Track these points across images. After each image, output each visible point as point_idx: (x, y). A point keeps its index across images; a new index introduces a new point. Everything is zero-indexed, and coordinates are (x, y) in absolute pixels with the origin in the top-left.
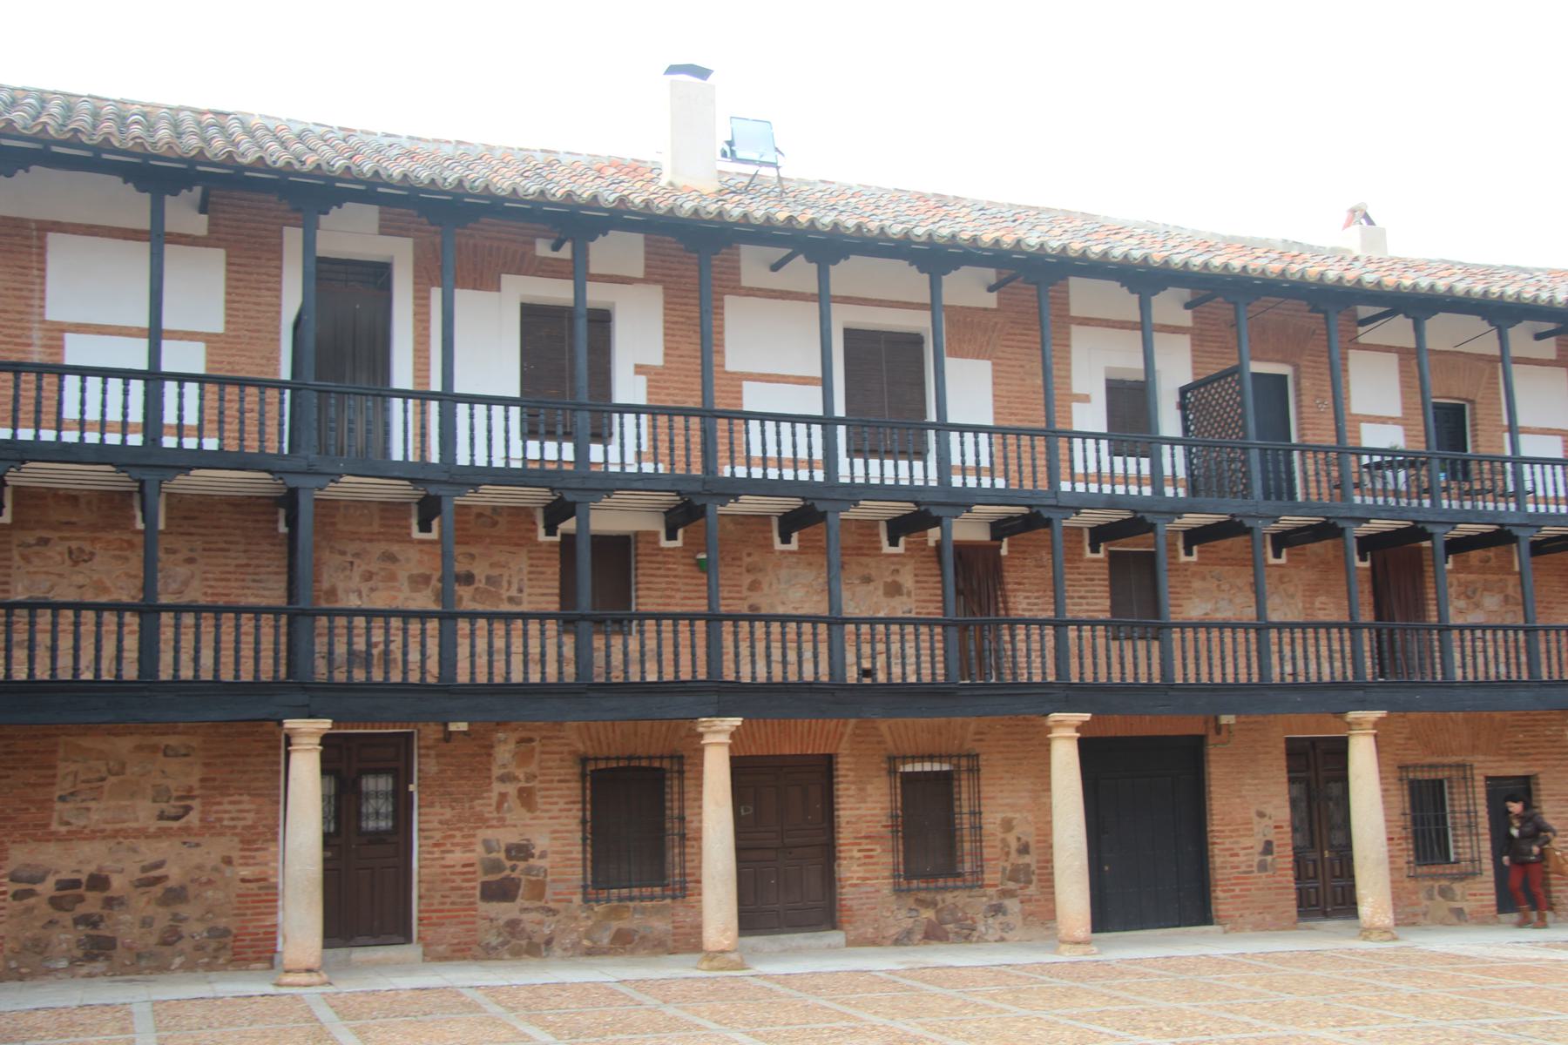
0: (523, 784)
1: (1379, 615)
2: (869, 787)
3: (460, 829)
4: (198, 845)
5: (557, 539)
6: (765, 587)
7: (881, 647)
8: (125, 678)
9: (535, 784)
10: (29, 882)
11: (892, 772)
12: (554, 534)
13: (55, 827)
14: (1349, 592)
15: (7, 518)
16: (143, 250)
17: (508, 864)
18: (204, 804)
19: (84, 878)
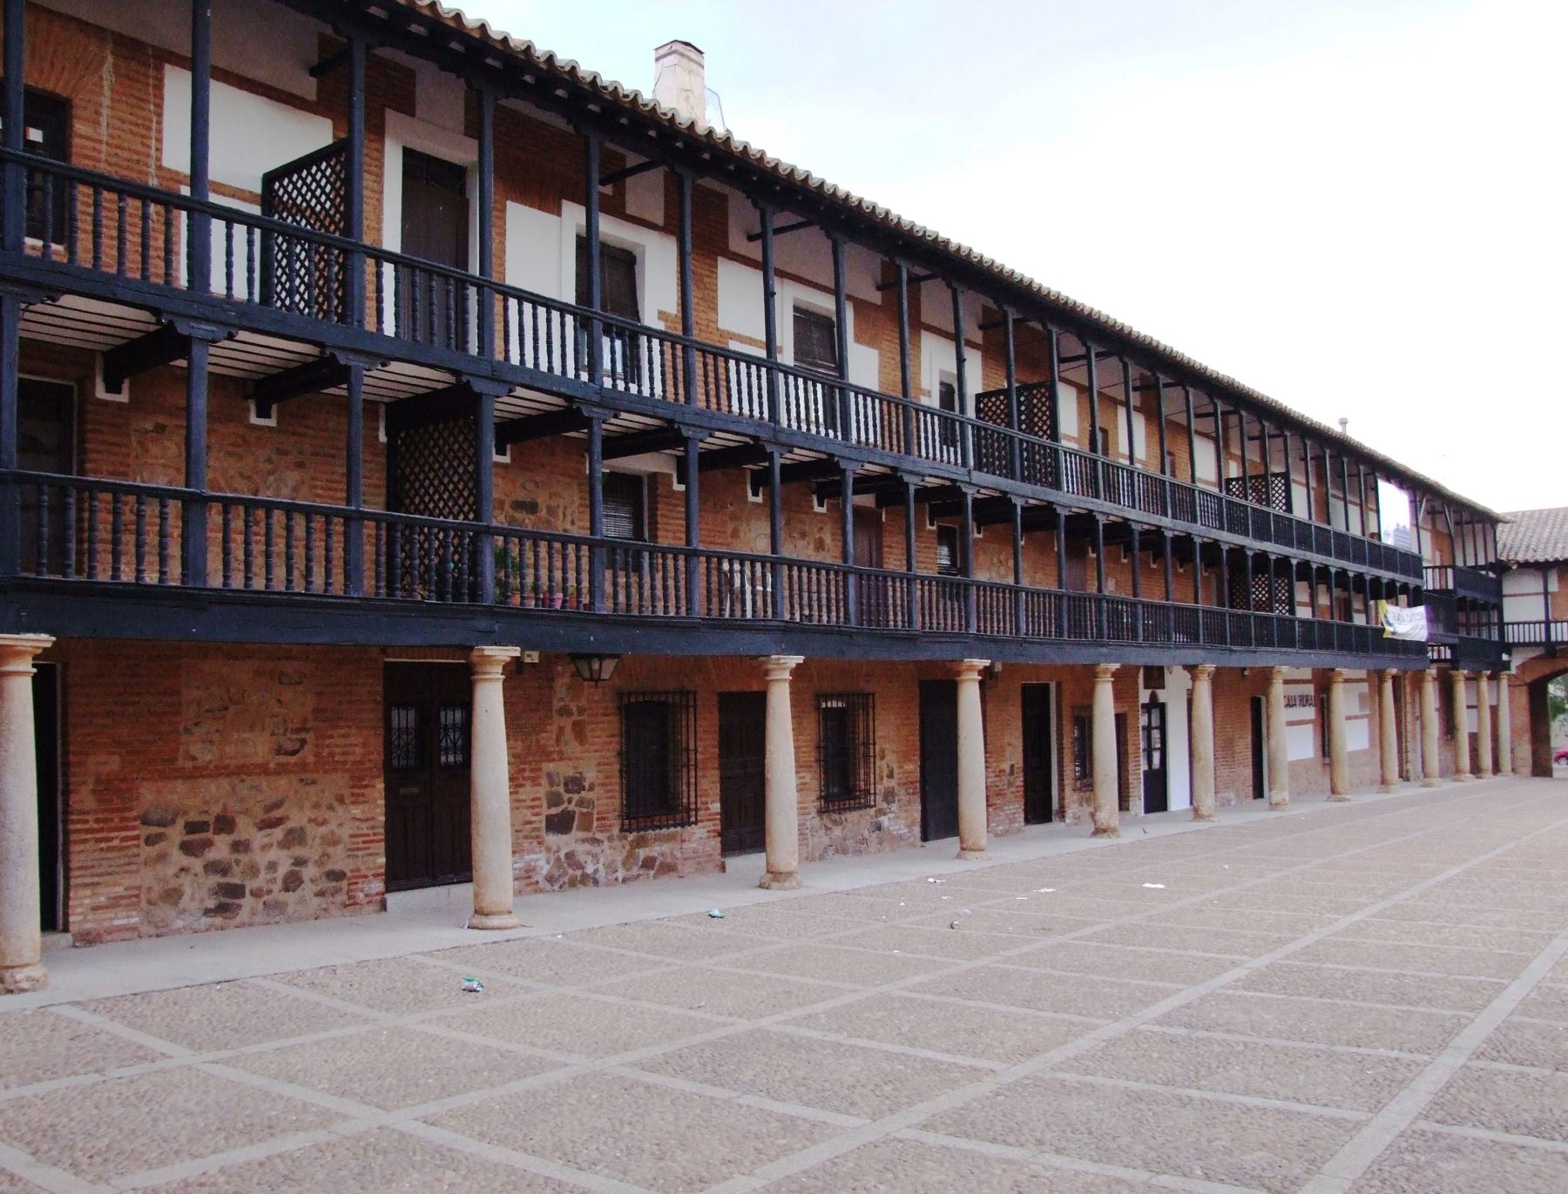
0: (576, 717)
1: (393, 502)
4: (314, 782)
9: (585, 717)
10: (159, 825)
11: (818, 708)
13: (180, 763)
14: (349, 475)
16: (758, 276)
17: (566, 796)
18: (317, 738)
19: (211, 819)
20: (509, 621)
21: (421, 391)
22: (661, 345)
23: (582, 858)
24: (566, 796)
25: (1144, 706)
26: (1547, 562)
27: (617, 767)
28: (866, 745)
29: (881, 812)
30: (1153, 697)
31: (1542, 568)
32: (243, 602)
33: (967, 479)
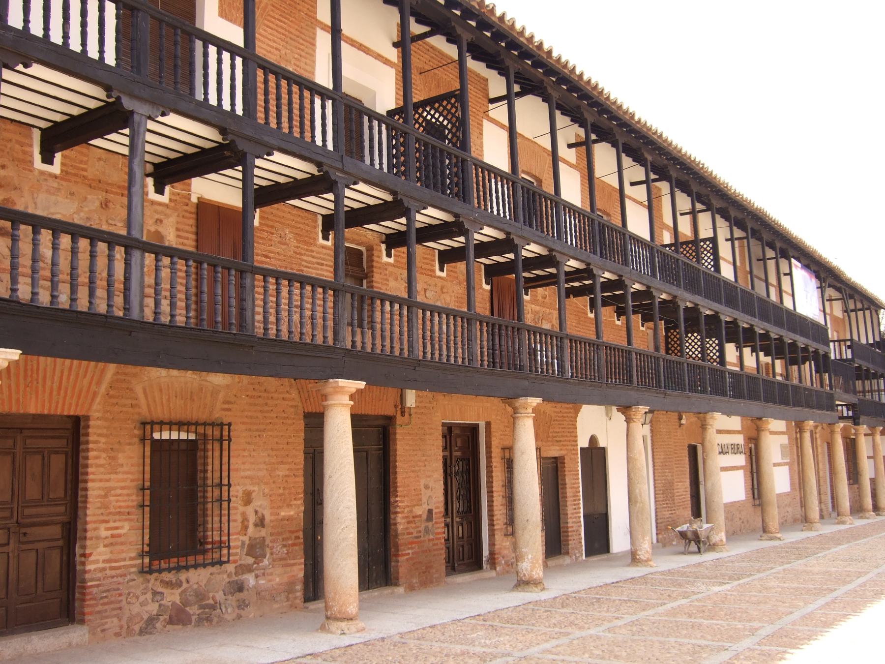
21: (282, 180)
33: (339, 166)
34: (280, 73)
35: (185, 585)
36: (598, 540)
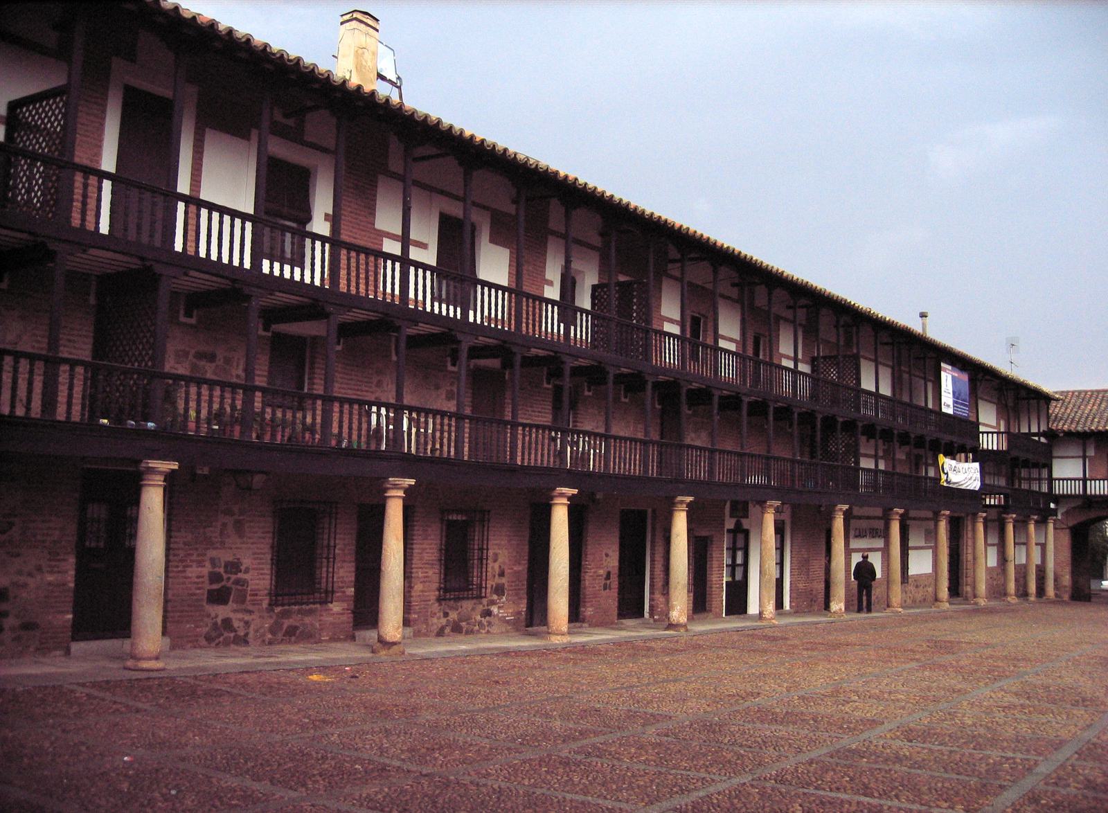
0: (236, 517)
1: (98, 351)
2: (430, 529)
3: (197, 549)
4: (18, 555)
5: (270, 334)
6: (385, 385)
7: (446, 434)
8: (73, 419)
11: (442, 520)
12: (268, 331)
15: (4, 286)
20: (171, 441)
22: (293, 238)
23: (236, 624)
24: (225, 576)
25: (729, 531)
26: (1085, 432)
27: (269, 557)
28: (481, 549)
29: (493, 603)
30: (738, 524)
31: (1082, 438)
32: (432, 462)
34: (359, 250)
35: (460, 610)
36: (737, 603)
